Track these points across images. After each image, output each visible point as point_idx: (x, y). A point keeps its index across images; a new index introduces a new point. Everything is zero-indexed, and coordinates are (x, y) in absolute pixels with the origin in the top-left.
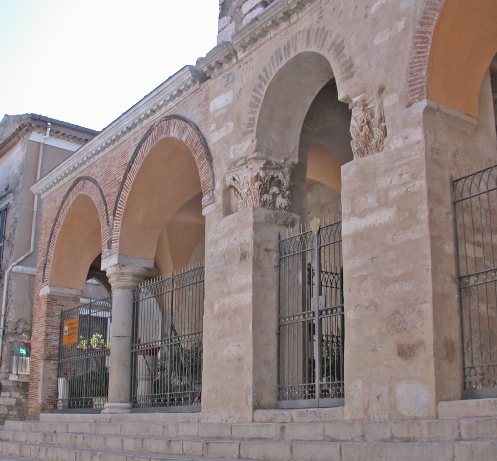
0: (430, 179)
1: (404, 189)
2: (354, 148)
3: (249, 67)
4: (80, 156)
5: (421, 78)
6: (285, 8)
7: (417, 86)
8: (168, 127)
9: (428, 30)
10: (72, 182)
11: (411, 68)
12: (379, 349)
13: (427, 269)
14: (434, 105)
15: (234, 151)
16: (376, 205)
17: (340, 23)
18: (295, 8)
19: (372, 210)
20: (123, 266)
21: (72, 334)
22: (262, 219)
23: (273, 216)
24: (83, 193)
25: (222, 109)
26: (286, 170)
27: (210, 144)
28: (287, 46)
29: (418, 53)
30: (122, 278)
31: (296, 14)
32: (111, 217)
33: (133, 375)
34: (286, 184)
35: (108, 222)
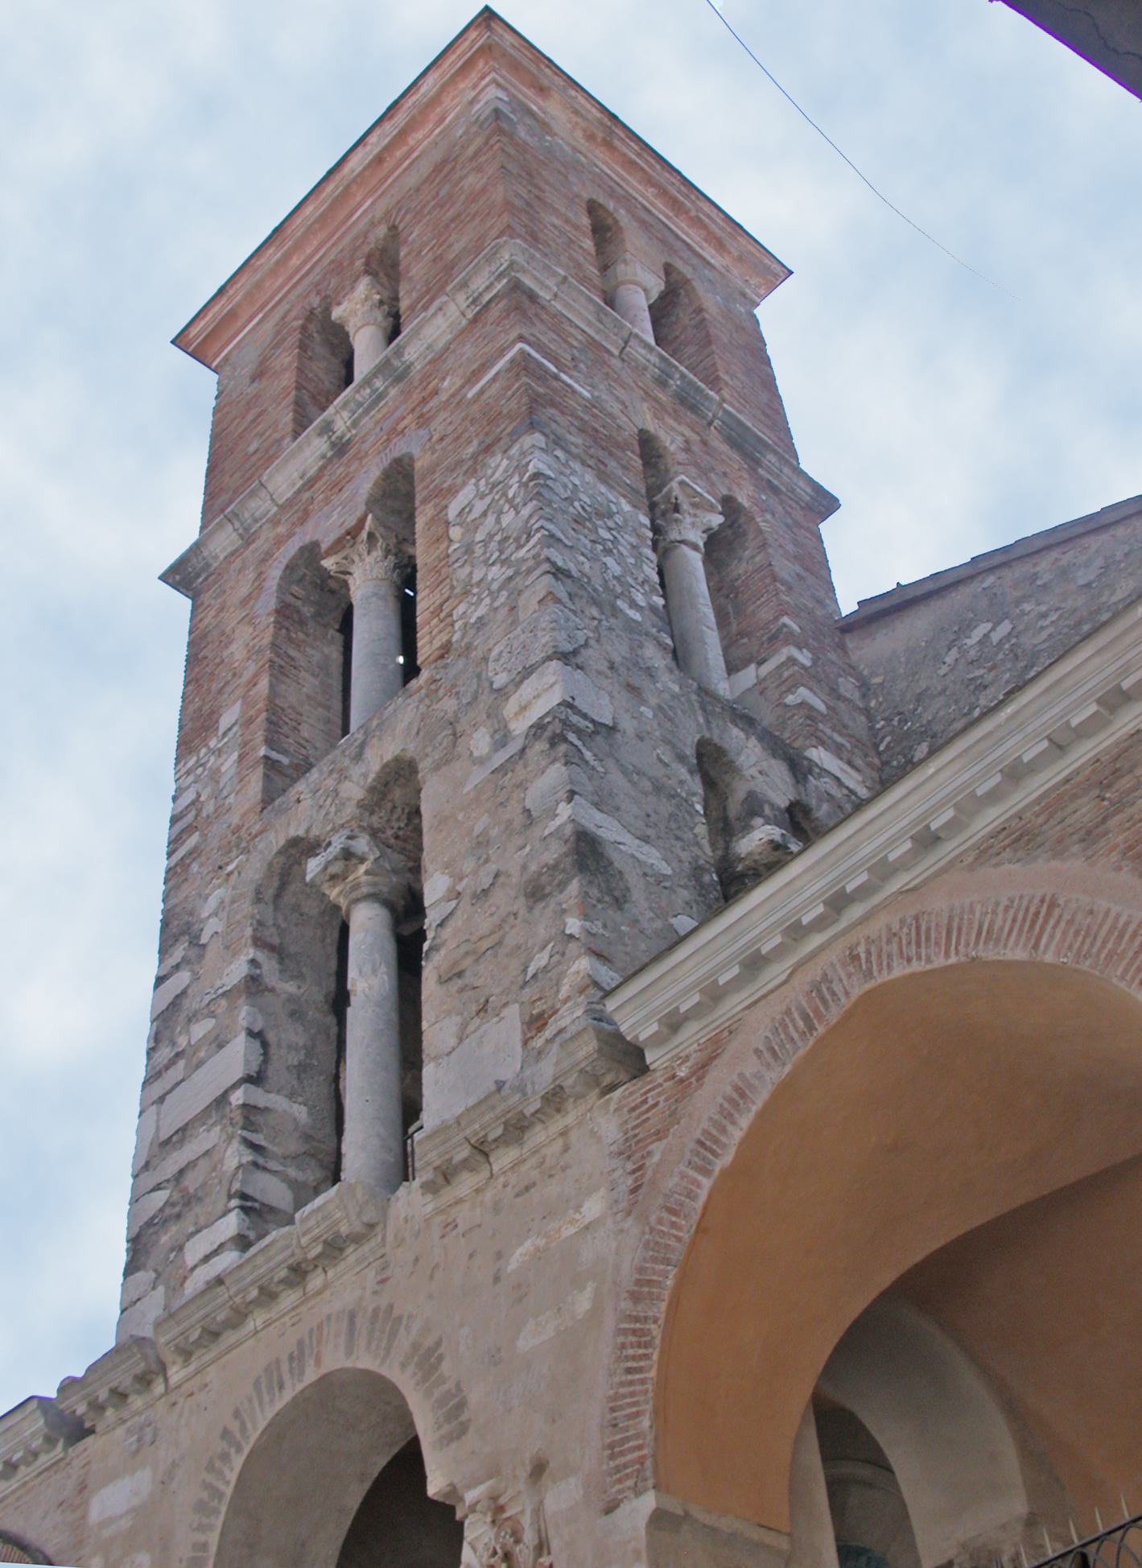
5: (637, 1436)
6: (293, 1255)
7: (629, 1457)
9: (650, 1314)
11: (613, 1410)
14: (675, 1506)
25: (121, 1517)
29: (629, 1371)
31: (319, 1270)
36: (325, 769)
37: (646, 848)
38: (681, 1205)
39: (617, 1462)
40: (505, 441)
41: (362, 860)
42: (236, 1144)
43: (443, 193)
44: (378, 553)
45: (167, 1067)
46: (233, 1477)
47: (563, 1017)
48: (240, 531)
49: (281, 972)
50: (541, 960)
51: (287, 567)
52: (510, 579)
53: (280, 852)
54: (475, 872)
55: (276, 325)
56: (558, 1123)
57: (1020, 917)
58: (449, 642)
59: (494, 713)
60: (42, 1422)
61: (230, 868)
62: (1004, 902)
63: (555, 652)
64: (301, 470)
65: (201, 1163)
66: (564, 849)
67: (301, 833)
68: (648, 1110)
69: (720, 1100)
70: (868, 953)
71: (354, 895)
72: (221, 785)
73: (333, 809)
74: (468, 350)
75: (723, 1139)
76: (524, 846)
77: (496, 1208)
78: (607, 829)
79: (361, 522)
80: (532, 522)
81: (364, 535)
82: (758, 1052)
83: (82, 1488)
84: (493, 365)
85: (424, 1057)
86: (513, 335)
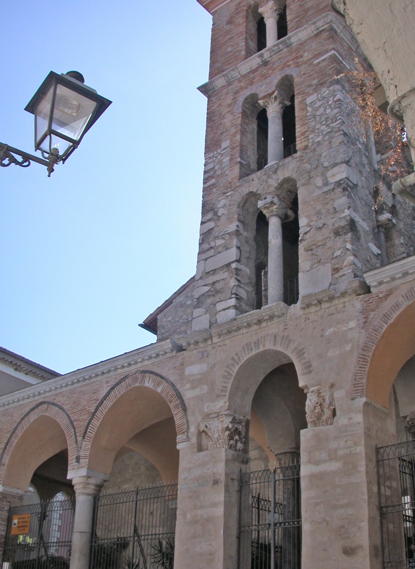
0: (366, 446)
1: (348, 450)
2: (308, 419)
3: (223, 350)
4: (48, 385)
5: (362, 383)
6: (260, 317)
7: (359, 388)
8: (143, 378)
9: (367, 355)
10: (34, 404)
11: (355, 376)
12: (329, 549)
13: (365, 502)
14: (369, 401)
15: (208, 407)
16: (328, 458)
17: (301, 336)
18: (267, 319)
19: (325, 461)
20: (89, 477)
21: (24, 526)
22: (230, 457)
23: (236, 455)
24: (47, 414)
25: (197, 375)
26: (244, 424)
27: (185, 399)
28: (256, 342)
29: (360, 367)
30: (87, 487)
31: (266, 322)
32: (80, 439)
33: (92, 562)
35: (76, 442)
36: (263, 173)
37: (364, 223)
38: (378, 329)
39: (356, 388)
40: (328, 84)
41: (275, 205)
44: (277, 103)
45: (207, 250)
46: (236, 371)
47: (344, 271)
48: (227, 80)
49: (244, 229)
50: (338, 253)
51: (245, 99)
52: (330, 132)
53: (246, 194)
54: (317, 221)
55: (236, 5)
56: (342, 300)
58: (307, 145)
59: (323, 174)
60: (171, 345)
61: (228, 194)
63: (344, 161)
64: (251, 66)
65: (221, 282)
66: (346, 223)
67: (254, 190)
68: (370, 303)
69: (391, 306)
72: (223, 166)
73: (266, 187)
74: (314, 45)
75: (391, 316)
76: (333, 218)
77: (322, 317)
78: (357, 219)
79: (273, 93)
80: (337, 115)
81: (274, 96)
82: (403, 296)
83: (182, 364)
84: (323, 55)
85: (299, 270)
86: (331, 47)
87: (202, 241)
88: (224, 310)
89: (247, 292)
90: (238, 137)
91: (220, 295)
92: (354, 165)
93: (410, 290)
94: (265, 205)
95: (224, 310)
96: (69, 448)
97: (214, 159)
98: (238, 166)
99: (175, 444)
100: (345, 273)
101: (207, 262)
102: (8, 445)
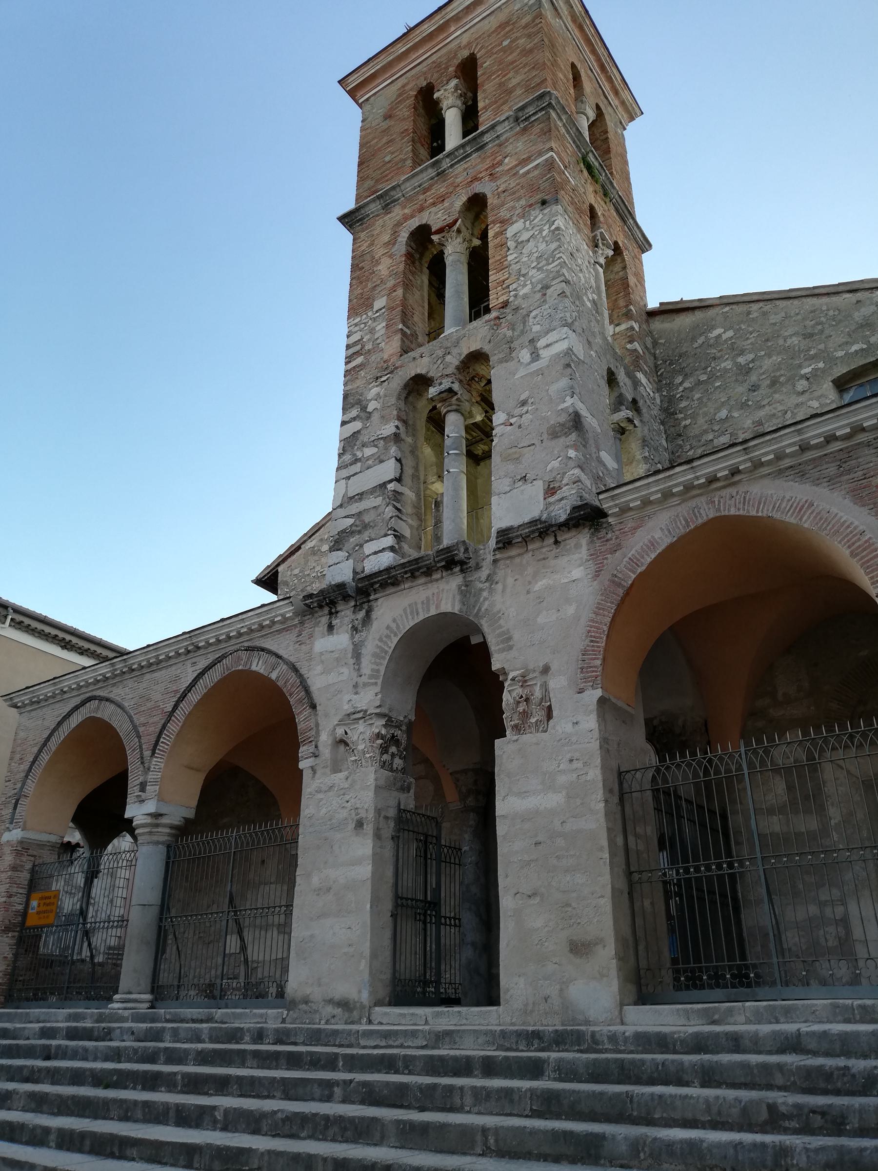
0: (604, 767)
2: (508, 724)
22: (382, 782)
26: (404, 728)
29: (592, 641)
34: (404, 742)
42: (390, 507)
43: (505, 43)
44: (460, 240)
55: (399, 89)
57: (795, 505)
62: (788, 497)
65: (372, 512)
67: (423, 372)
70: (719, 502)
71: (449, 408)
78: (584, 412)
79: (456, 221)
81: (455, 228)
82: (661, 528)
87: (343, 450)
88: (376, 553)
89: (411, 527)
90: (400, 292)
91: (370, 531)
92: (579, 330)
93: (674, 520)
94: (439, 394)
95: (376, 553)
96: (130, 769)
97: (363, 326)
98: (399, 336)
99: (297, 760)
100: (565, 495)
101: (350, 482)
102: (35, 765)
